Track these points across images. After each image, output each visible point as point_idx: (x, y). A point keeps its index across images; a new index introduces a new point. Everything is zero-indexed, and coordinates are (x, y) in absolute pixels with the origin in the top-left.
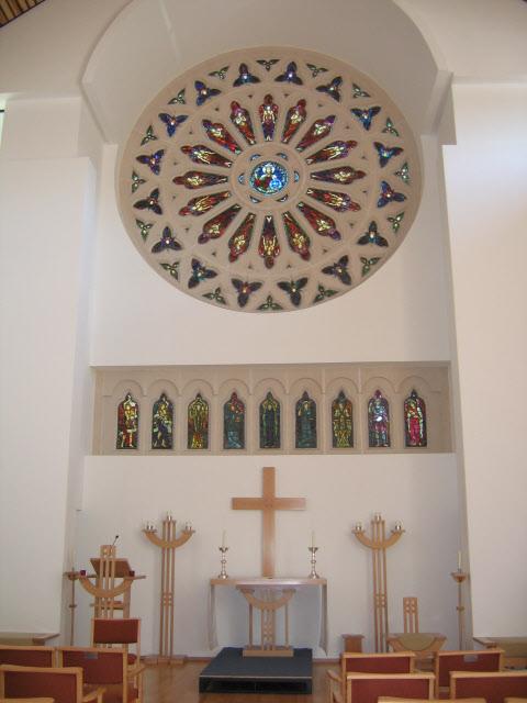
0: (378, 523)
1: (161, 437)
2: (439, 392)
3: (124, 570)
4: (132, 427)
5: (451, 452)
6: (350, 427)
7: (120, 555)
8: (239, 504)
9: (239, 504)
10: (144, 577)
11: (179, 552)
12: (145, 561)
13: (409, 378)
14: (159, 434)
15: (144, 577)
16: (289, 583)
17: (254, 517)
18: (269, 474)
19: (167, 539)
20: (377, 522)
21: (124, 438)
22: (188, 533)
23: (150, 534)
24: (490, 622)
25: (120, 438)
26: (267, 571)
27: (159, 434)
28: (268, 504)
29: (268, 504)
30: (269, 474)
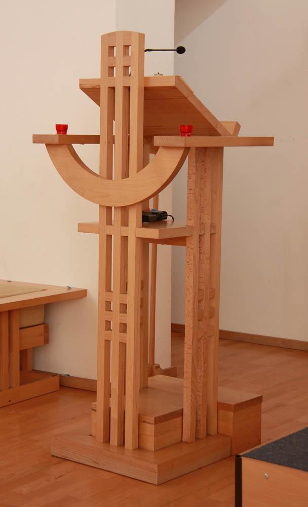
6: (207, 220)
10: (267, 142)
15: (267, 142)
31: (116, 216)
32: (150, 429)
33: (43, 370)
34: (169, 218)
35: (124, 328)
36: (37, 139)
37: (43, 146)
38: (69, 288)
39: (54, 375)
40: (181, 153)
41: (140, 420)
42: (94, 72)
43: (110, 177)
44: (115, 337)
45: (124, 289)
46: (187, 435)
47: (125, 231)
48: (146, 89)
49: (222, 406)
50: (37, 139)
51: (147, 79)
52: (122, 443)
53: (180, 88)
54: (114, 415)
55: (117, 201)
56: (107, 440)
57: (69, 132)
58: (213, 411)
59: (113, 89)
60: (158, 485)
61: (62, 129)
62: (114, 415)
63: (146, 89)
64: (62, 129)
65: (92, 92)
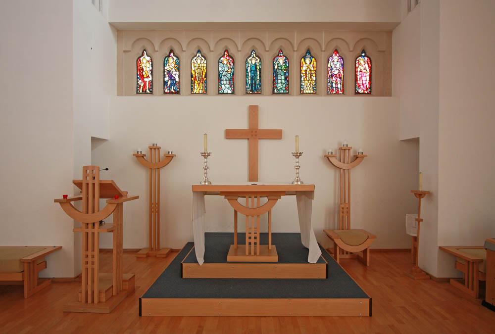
0: (155, 149)
1: (171, 84)
2: (384, 51)
3: (110, 191)
4: (148, 77)
5: (391, 96)
6: (119, 223)
7: (105, 177)
8: (231, 134)
9: (231, 134)
10: (137, 197)
11: (163, 172)
12: (132, 182)
13: (362, 39)
14: (169, 82)
15: (137, 197)
16: (336, 221)
17: (242, 145)
18: (253, 111)
19: (154, 161)
20: (154, 148)
21: (142, 85)
22: (170, 157)
23: (139, 157)
24: (450, 223)
25: (138, 86)
26: (253, 175)
27: (169, 82)
28: (253, 134)
29: (253, 134)
30: (253, 111)
31: (90, 226)
32: (103, 295)
33: (43, 277)
34: (103, 223)
35: (93, 263)
36: (56, 201)
37: (58, 203)
38: (55, 247)
39: (49, 279)
40: (115, 205)
41: (100, 292)
42: (80, 178)
43: (88, 213)
44: (90, 266)
45: (93, 250)
46: (114, 293)
47: (93, 230)
48: (100, 184)
49: (124, 281)
50: (56, 201)
51: (100, 181)
52: (93, 301)
53: (113, 183)
54: (90, 293)
55: (91, 221)
56: (87, 301)
57: (69, 197)
58: (121, 282)
59: (88, 184)
60: (110, 313)
61: (65, 197)
62: (90, 293)
63: (100, 184)
64: (65, 197)
65: (78, 184)
